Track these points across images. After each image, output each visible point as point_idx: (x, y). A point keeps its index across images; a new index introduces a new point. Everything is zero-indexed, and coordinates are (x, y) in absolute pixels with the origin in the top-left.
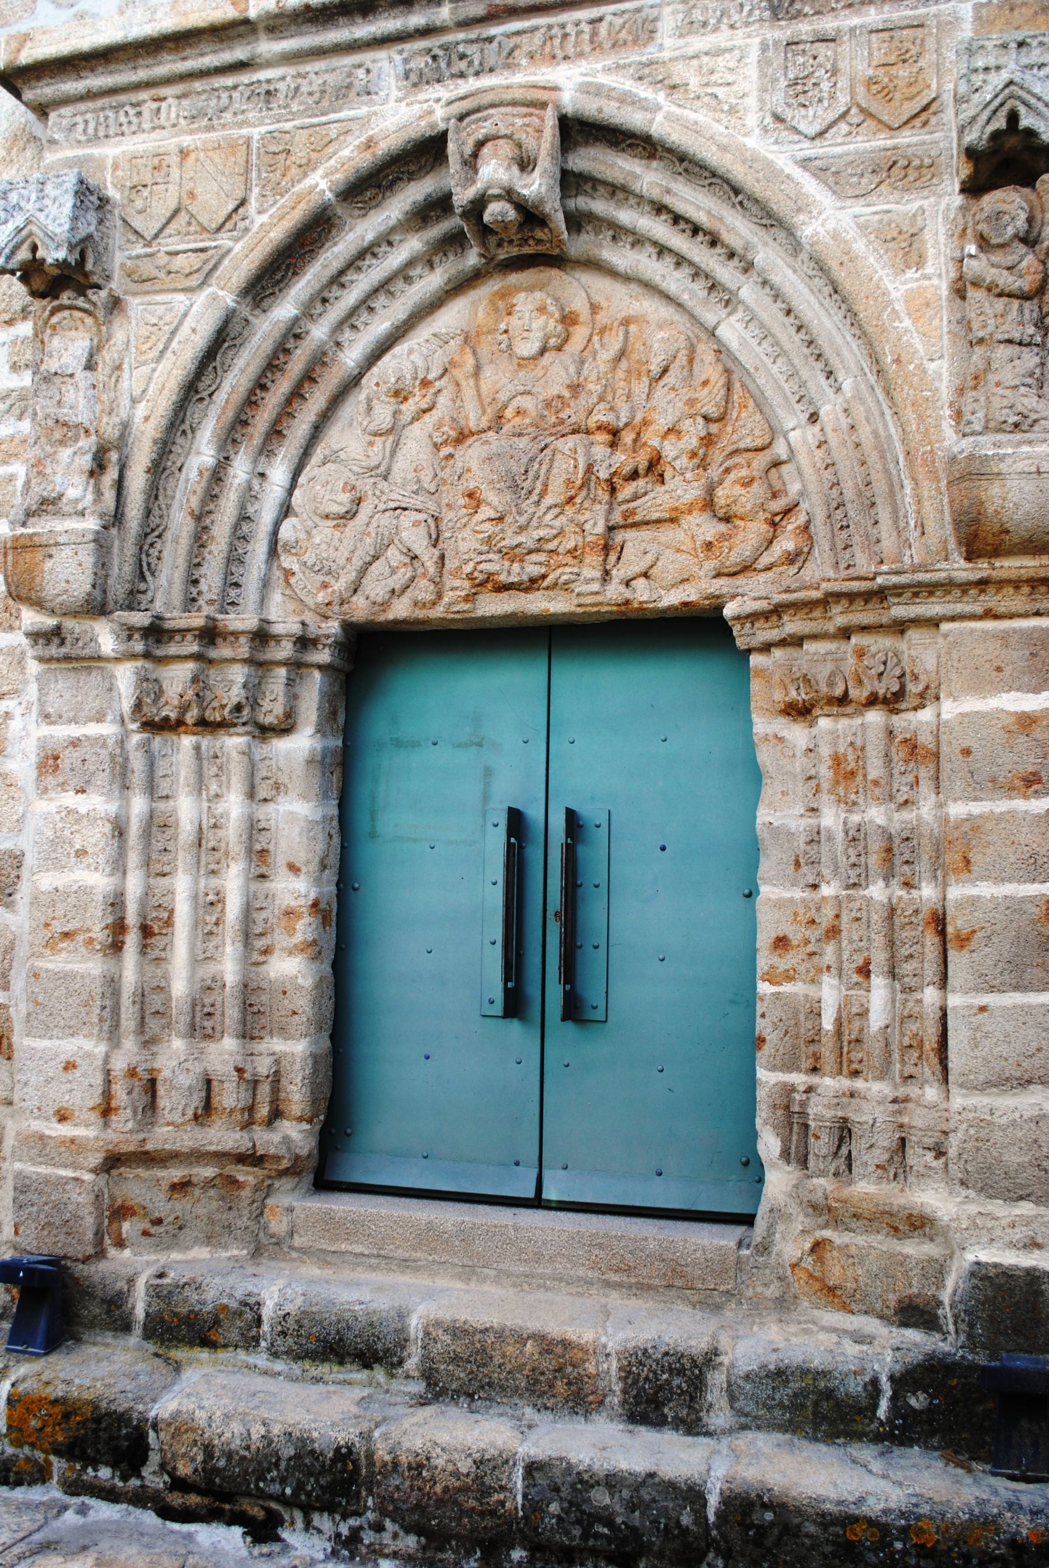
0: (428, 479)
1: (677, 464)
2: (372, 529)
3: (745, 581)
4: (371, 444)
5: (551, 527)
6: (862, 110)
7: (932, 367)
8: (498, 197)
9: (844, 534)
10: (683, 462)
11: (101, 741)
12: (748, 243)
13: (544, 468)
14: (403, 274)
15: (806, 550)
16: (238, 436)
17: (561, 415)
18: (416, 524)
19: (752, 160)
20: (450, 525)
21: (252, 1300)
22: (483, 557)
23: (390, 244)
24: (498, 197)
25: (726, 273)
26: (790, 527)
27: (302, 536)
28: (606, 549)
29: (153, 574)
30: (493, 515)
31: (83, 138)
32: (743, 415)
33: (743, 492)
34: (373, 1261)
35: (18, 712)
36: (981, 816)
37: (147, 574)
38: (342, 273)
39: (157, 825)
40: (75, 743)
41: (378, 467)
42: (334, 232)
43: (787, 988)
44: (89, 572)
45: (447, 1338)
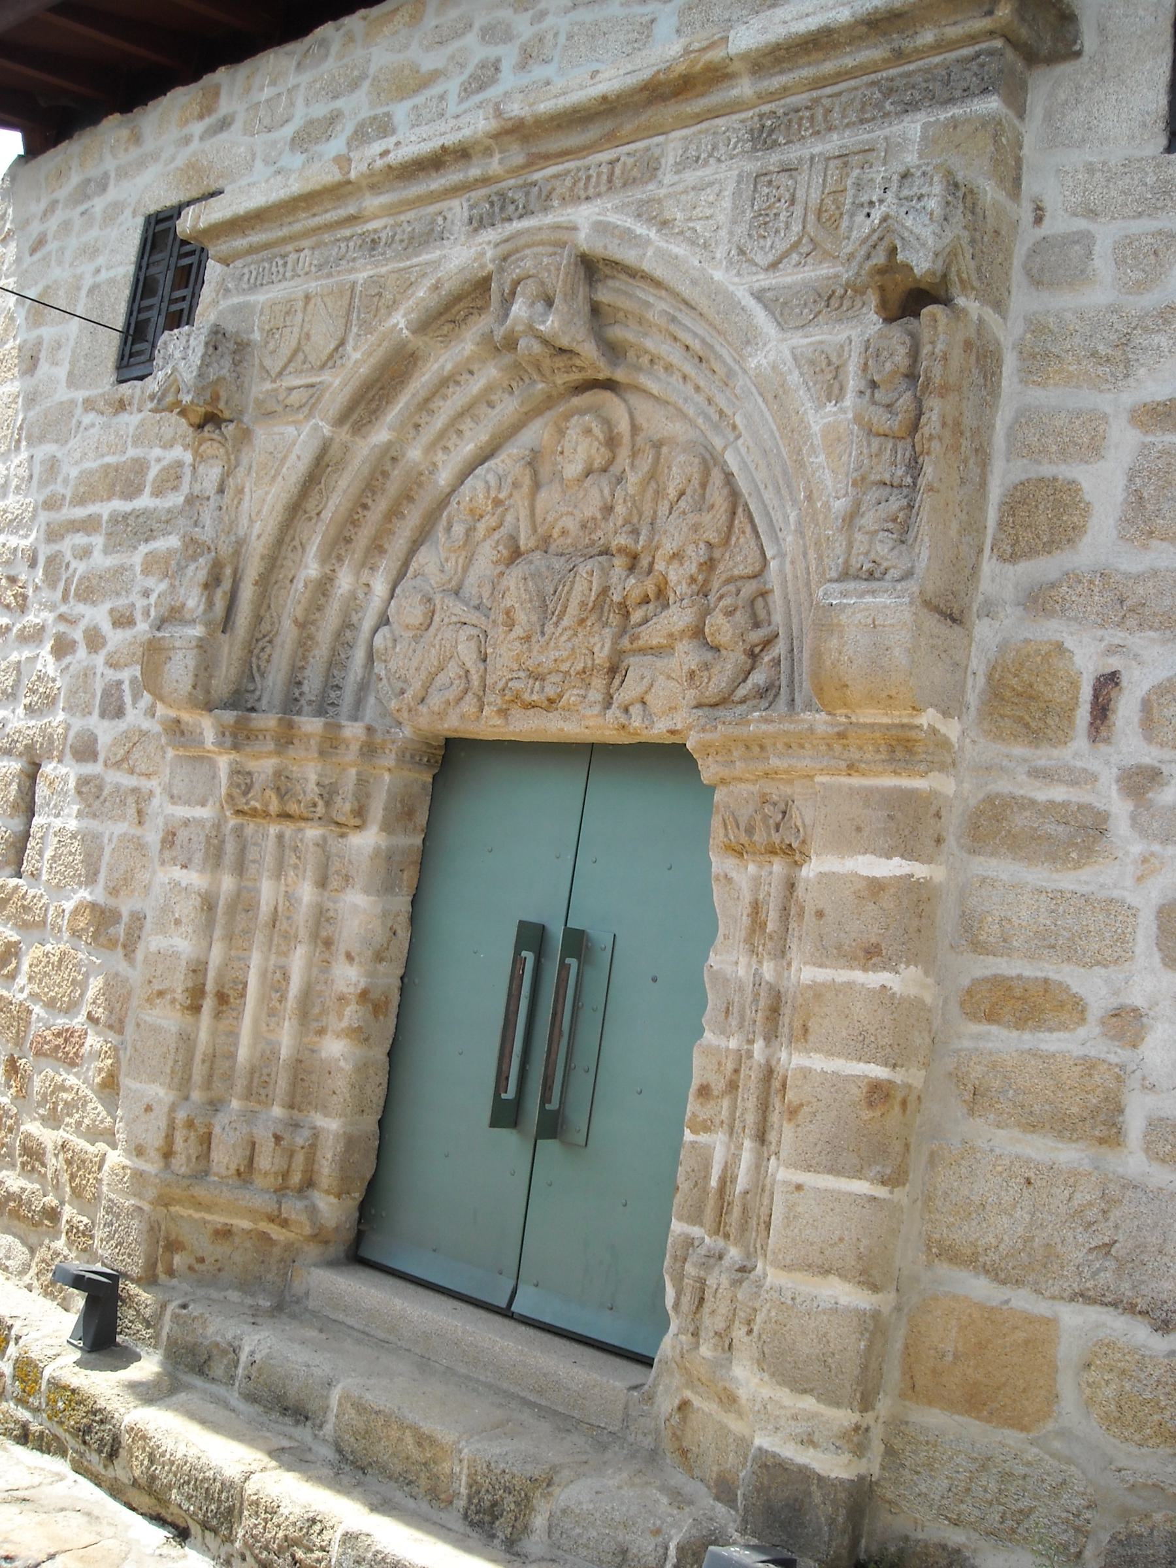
10: (683, 588)
11: (200, 822)
14: (486, 398)
23: (471, 373)
26: (766, 659)
29: (262, 676)
31: (245, 286)
36: (823, 984)
37: (257, 675)
38: (427, 400)
39: (244, 903)
40: (186, 823)
42: (420, 363)
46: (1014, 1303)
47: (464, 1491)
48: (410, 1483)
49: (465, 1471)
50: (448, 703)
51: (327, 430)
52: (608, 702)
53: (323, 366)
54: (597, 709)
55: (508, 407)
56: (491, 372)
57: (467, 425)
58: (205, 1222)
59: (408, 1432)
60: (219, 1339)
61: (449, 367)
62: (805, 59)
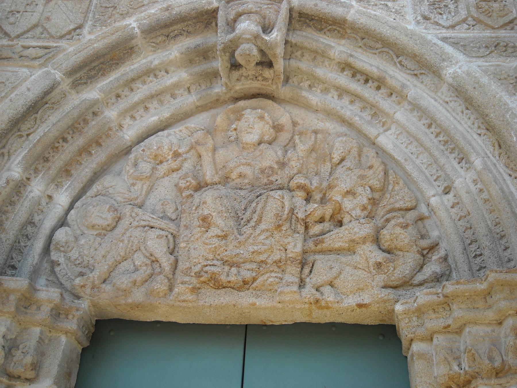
0: (171, 210)
1: (354, 214)
2: (125, 238)
3: (404, 292)
4: (133, 185)
5: (264, 244)
8: (248, 41)
9: (478, 260)
10: (358, 212)
12: (404, 84)
13: (260, 206)
14: (172, 91)
15: (447, 272)
16: (40, 167)
17: (270, 179)
18: (159, 237)
19: (411, 35)
20: (186, 239)
22: (209, 262)
23: (167, 72)
24: (248, 41)
25: (386, 104)
27: (72, 239)
28: (303, 264)
30: (220, 233)
32: (397, 188)
33: (402, 231)
38: (133, 80)
41: (137, 198)
50: (134, 283)
51: (58, 75)
52: (302, 284)
53: (61, 37)
54: (295, 288)
55: (188, 100)
56: (183, 75)
57: (153, 105)
61: (156, 62)
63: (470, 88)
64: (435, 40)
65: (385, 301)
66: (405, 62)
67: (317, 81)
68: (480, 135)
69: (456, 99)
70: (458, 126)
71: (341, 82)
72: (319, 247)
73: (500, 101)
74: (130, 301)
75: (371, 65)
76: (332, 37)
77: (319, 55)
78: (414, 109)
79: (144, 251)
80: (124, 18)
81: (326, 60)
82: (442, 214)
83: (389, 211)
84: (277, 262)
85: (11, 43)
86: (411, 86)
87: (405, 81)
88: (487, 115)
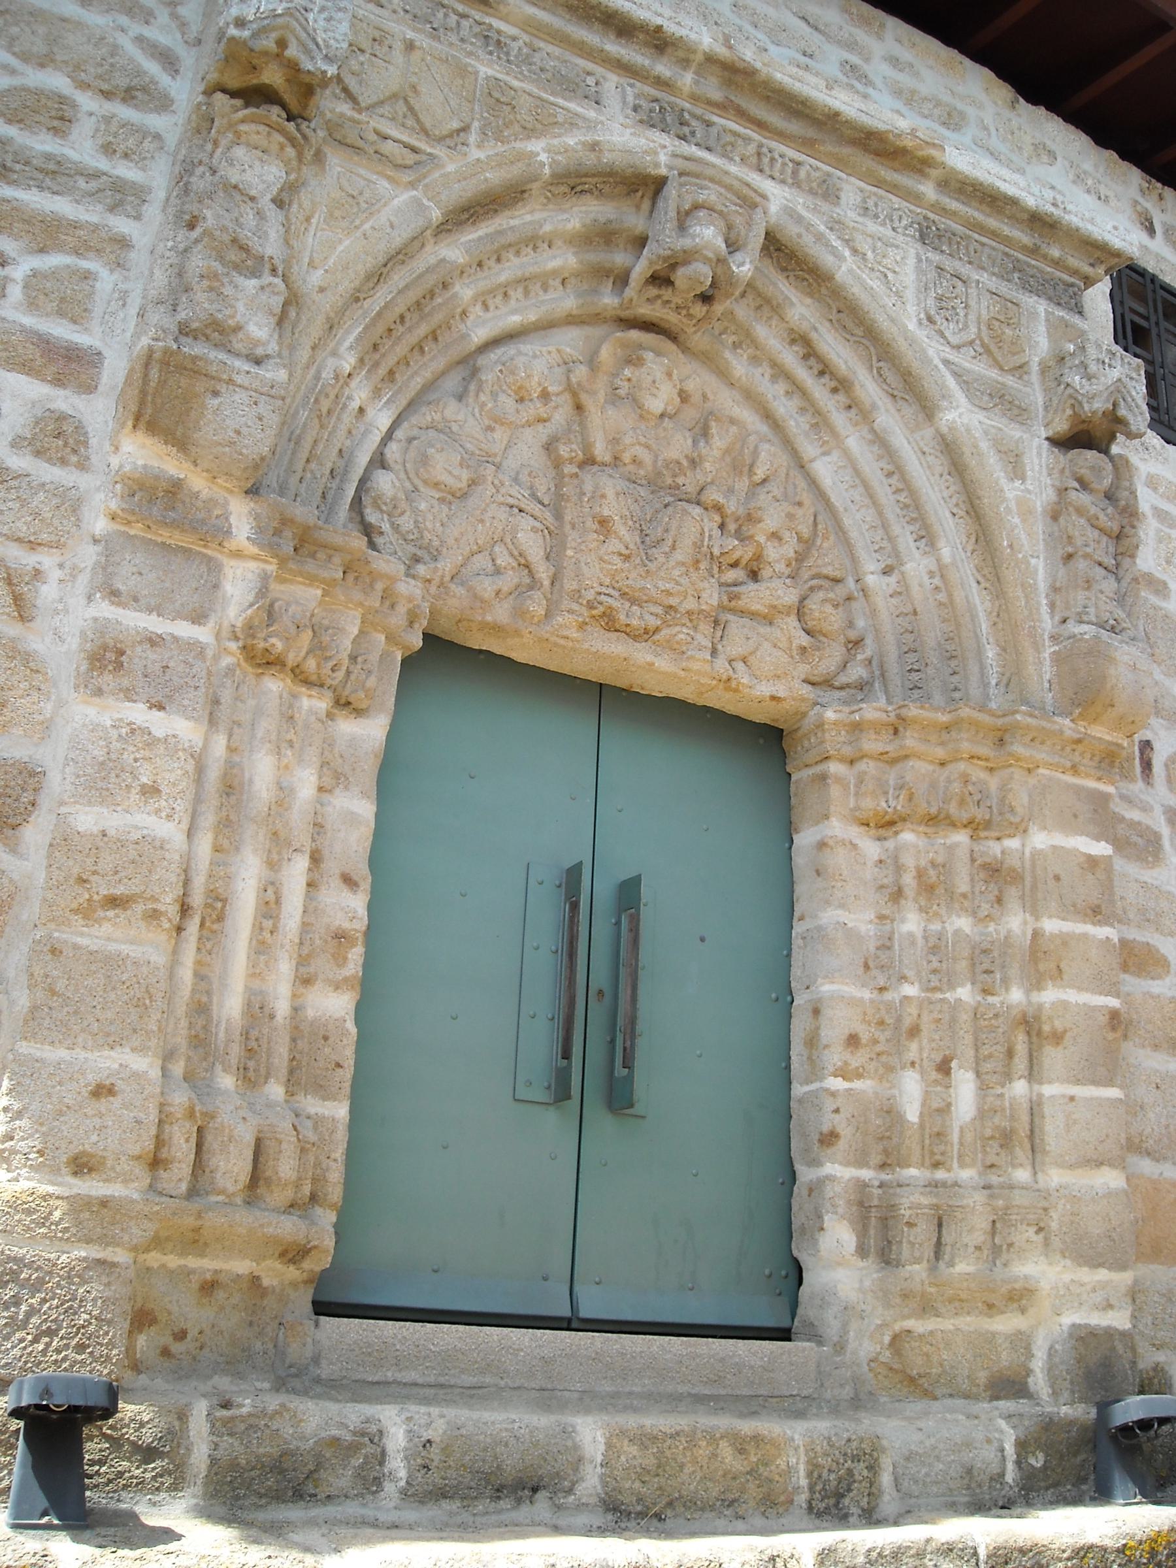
5: (677, 583)
6: (983, 345)
7: (1033, 561)
8: (706, 260)
10: (780, 567)
14: (544, 280)
18: (534, 530)
20: (574, 544)
21: (374, 1428)
22: (604, 590)
24: (706, 260)
25: (839, 419)
33: (834, 612)
34: (430, 1392)
35: (56, 574)
36: (1067, 934)
40: (154, 641)
43: (858, 1085)
44: (271, 432)
45: (634, 1450)
46: (1166, 1174)
47: (804, 1482)
48: (732, 1503)
49: (803, 1458)
53: (441, 139)
56: (564, 259)
58: (191, 1272)
59: (723, 1444)
60: (335, 1432)
61: (548, 228)
62: (978, 205)
63: (967, 451)
64: (937, 361)
65: (803, 700)
66: (886, 373)
67: (748, 341)
68: (954, 515)
69: (939, 454)
70: (930, 492)
71: (786, 360)
72: (733, 603)
73: (997, 483)
74: (489, 618)
75: (839, 357)
76: (796, 287)
77: (769, 306)
78: (875, 442)
79: (511, 546)
80: (529, 138)
81: (776, 317)
82: (880, 602)
83: (813, 578)
84: (689, 613)
85: (356, 116)
86: (883, 410)
87: (876, 399)
88: (979, 498)
